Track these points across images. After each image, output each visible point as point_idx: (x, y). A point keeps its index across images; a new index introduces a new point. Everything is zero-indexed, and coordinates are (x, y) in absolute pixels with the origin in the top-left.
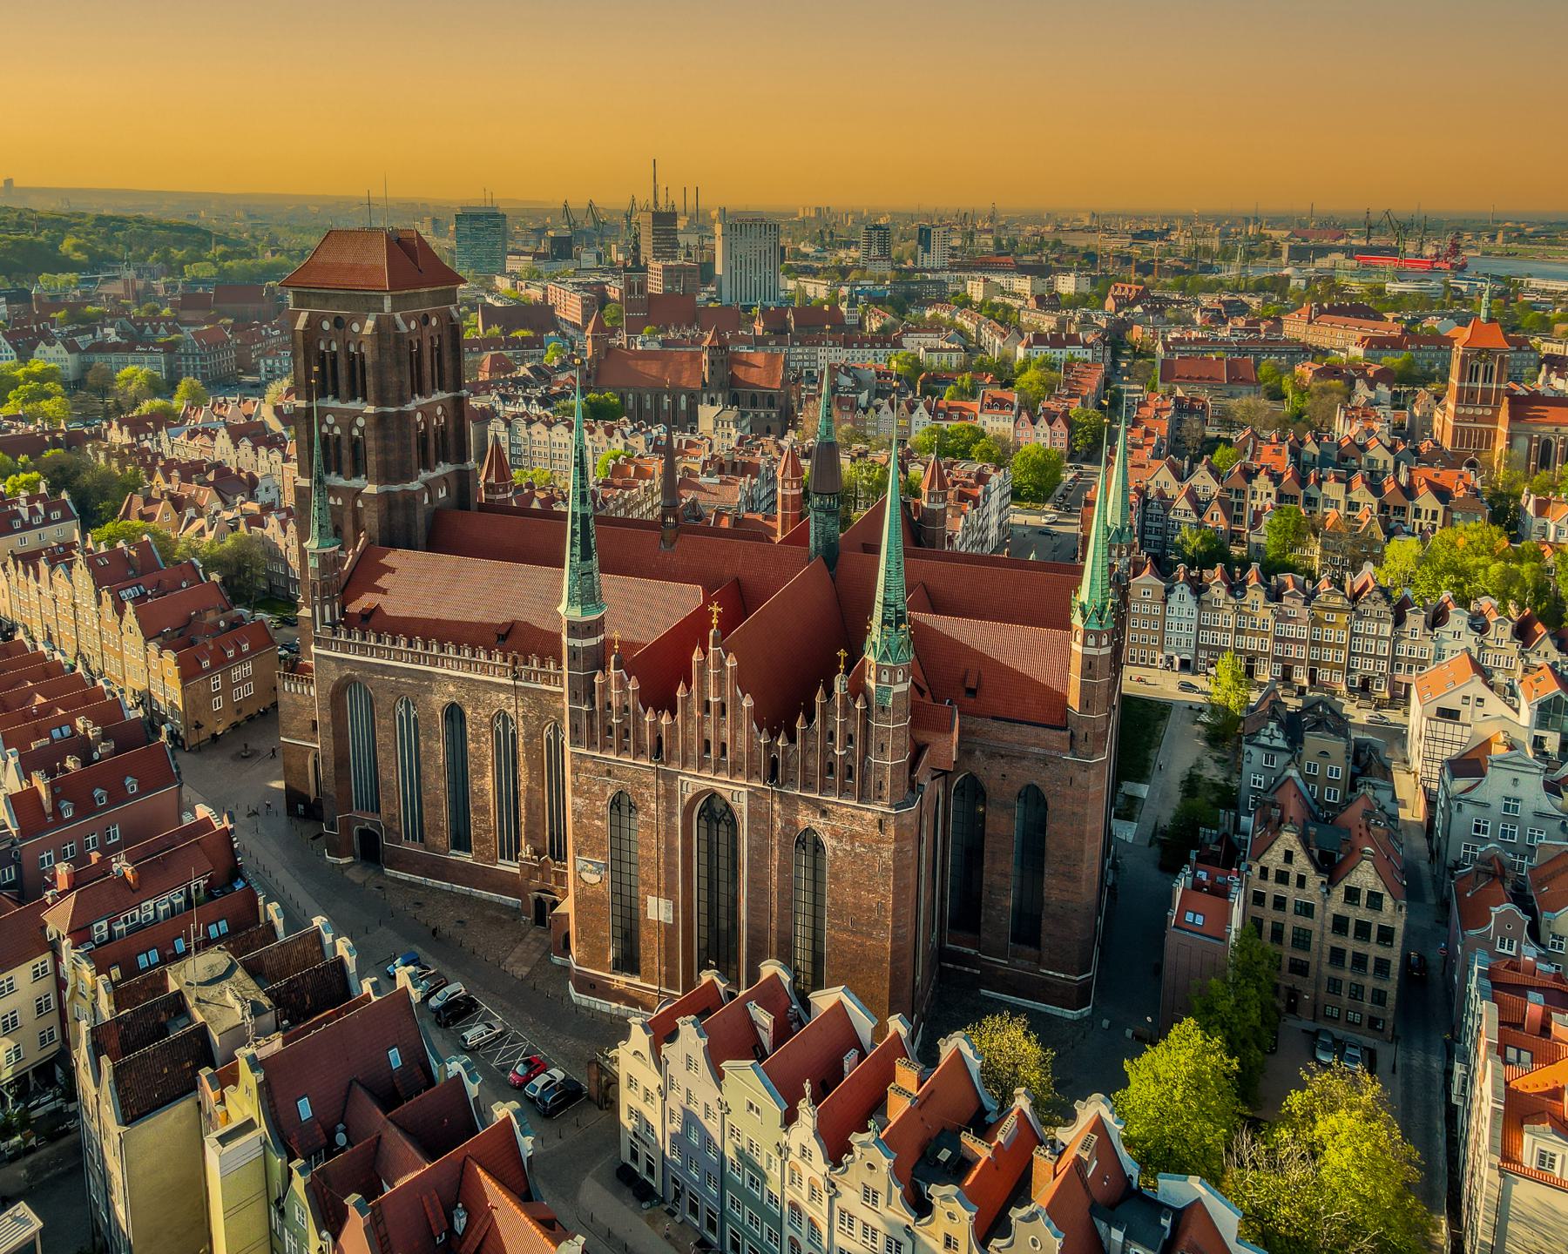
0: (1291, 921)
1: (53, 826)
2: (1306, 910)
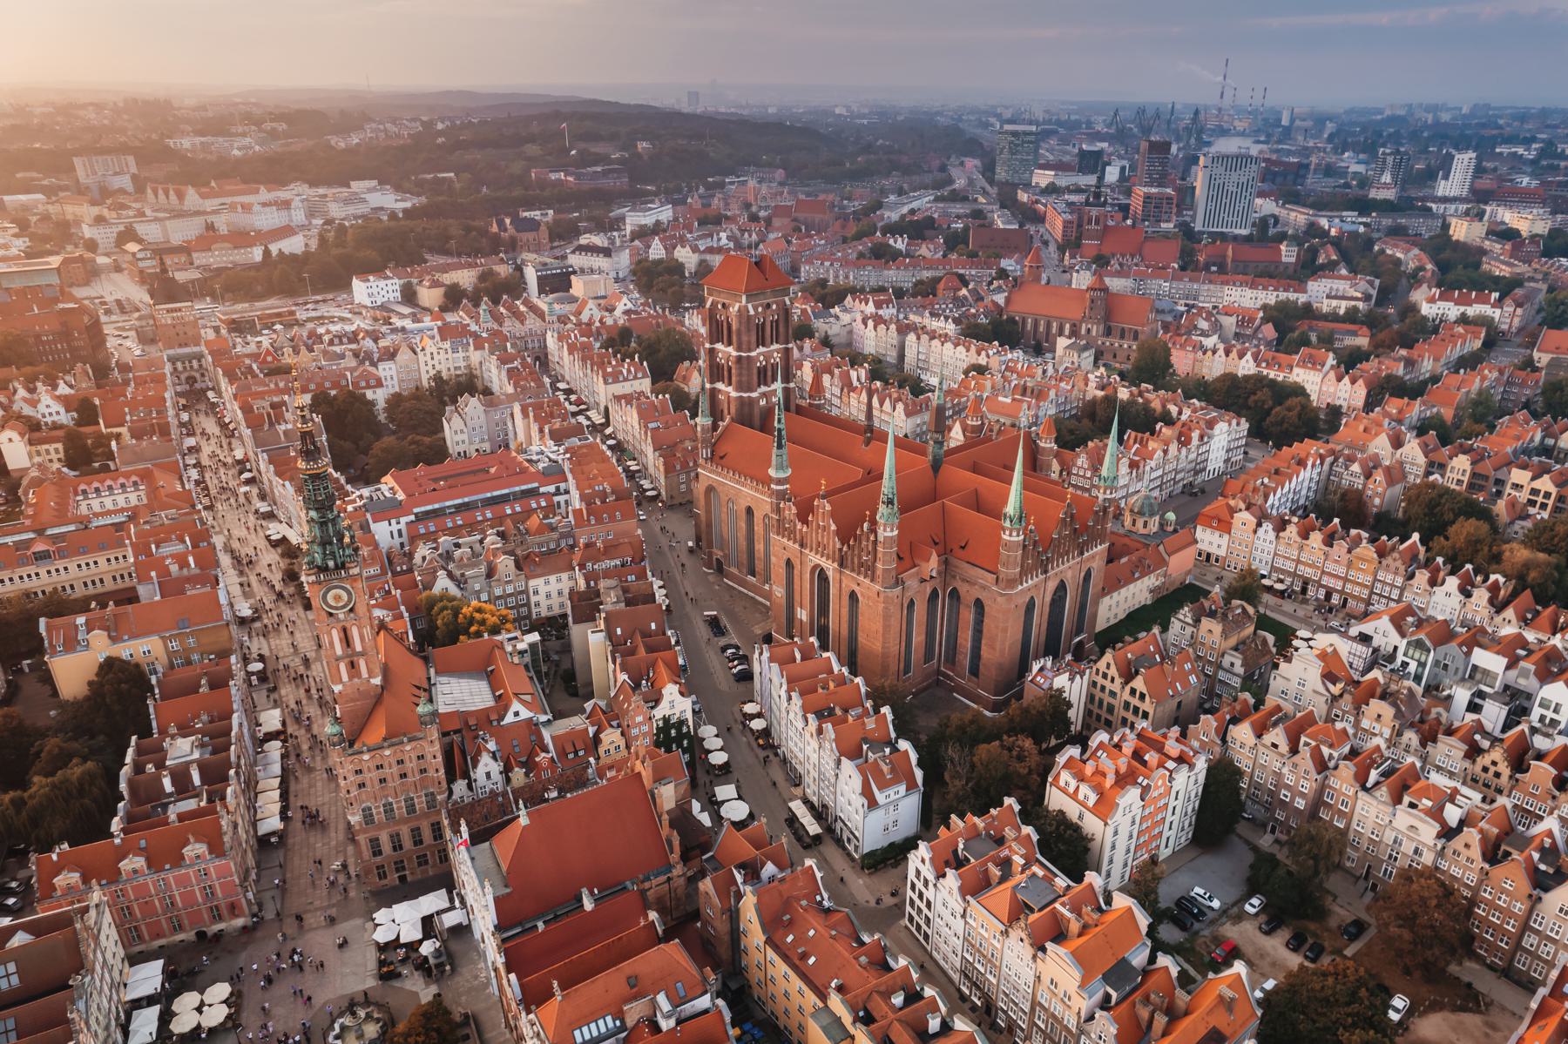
0: (1107, 699)
2: (1113, 694)
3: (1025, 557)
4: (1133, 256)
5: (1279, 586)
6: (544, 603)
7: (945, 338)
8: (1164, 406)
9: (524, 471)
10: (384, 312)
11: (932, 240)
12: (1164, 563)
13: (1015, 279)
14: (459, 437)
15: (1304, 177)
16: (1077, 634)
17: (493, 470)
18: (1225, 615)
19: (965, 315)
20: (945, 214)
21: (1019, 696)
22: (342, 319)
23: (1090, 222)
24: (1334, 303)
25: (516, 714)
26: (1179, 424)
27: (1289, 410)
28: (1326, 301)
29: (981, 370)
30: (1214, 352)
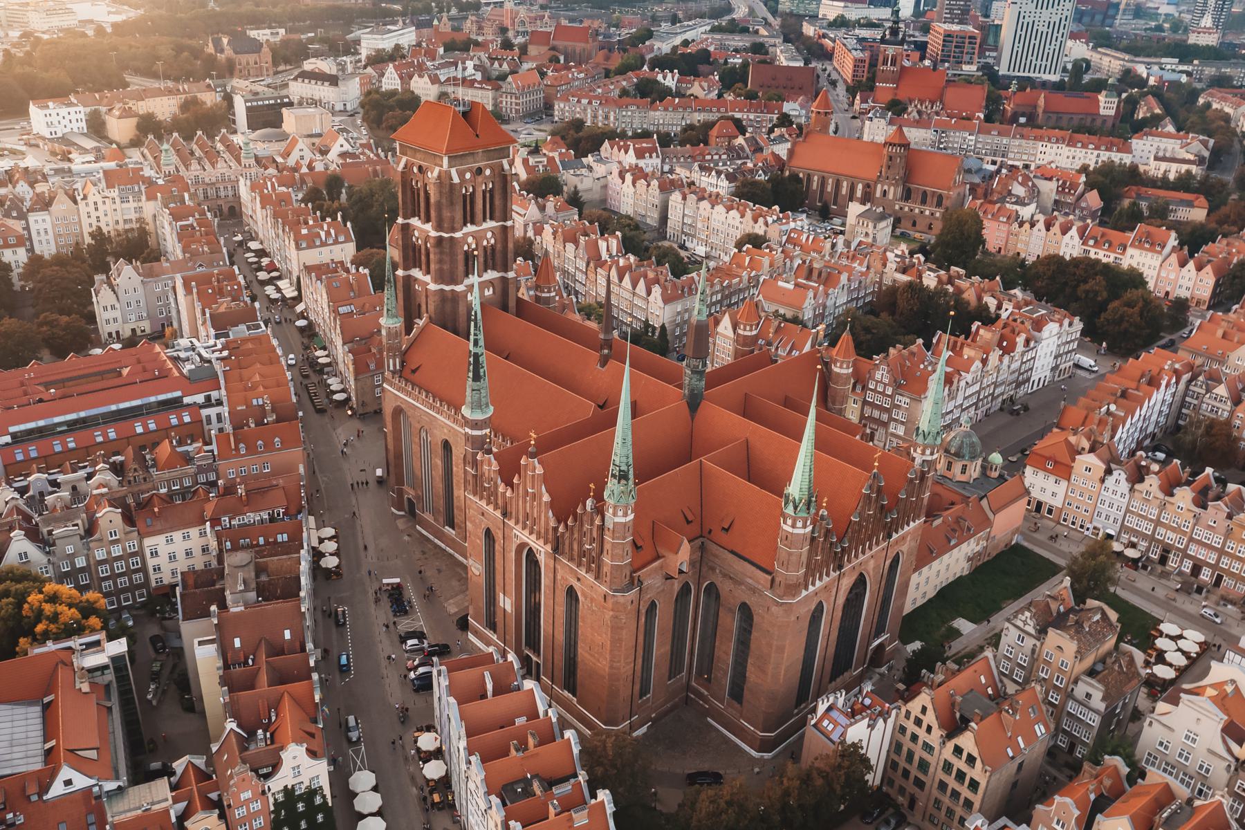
0: (919, 753)
1: (235, 456)
2: (928, 747)
3: (812, 552)
4: (933, 103)
5: (1131, 553)
6: (166, 567)
7: (715, 200)
8: (980, 298)
9: (165, 375)
10: (63, 147)
11: (706, 76)
12: (987, 523)
13: (800, 127)
14: (109, 315)
15: (1114, 18)
16: (877, 635)
17: (125, 371)
18: (1079, 624)
19: (740, 170)
20: (722, 47)
21: (794, 754)
22: (13, 152)
23: (885, 63)
24: (1164, 166)
25: (68, 783)
26: (1000, 323)
27: (1130, 305)
28: (1153, 164)
29: (757, 241)
30: (1033, 225)
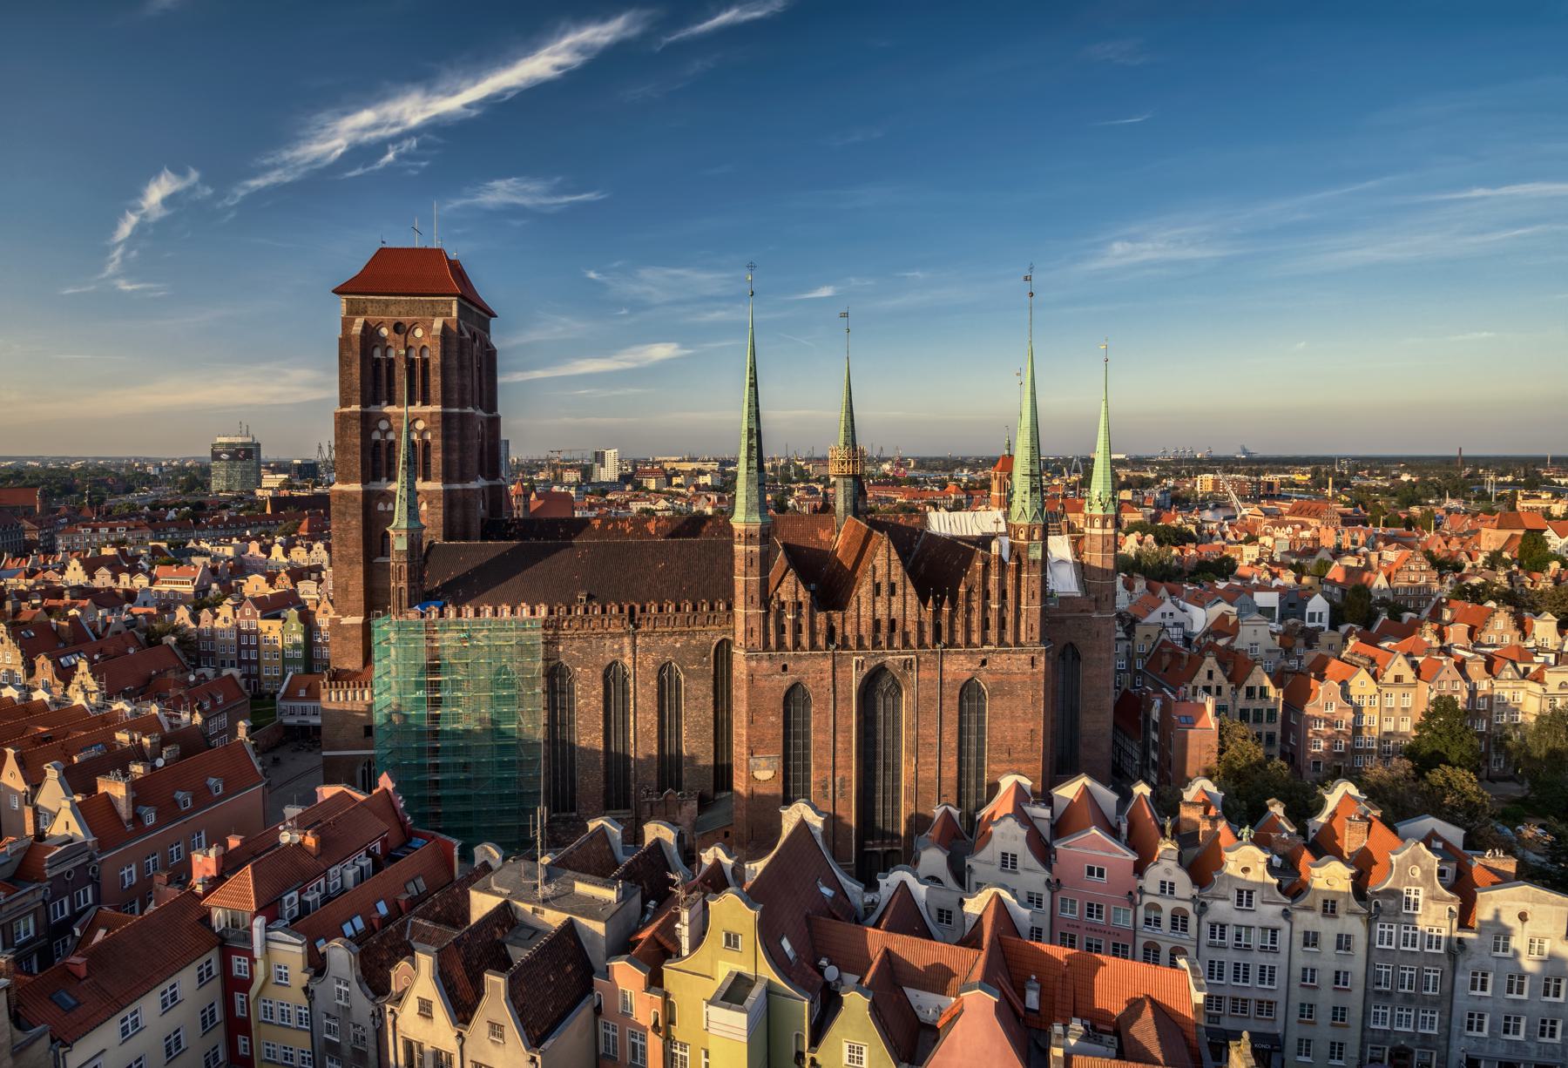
1: (132, 837)
